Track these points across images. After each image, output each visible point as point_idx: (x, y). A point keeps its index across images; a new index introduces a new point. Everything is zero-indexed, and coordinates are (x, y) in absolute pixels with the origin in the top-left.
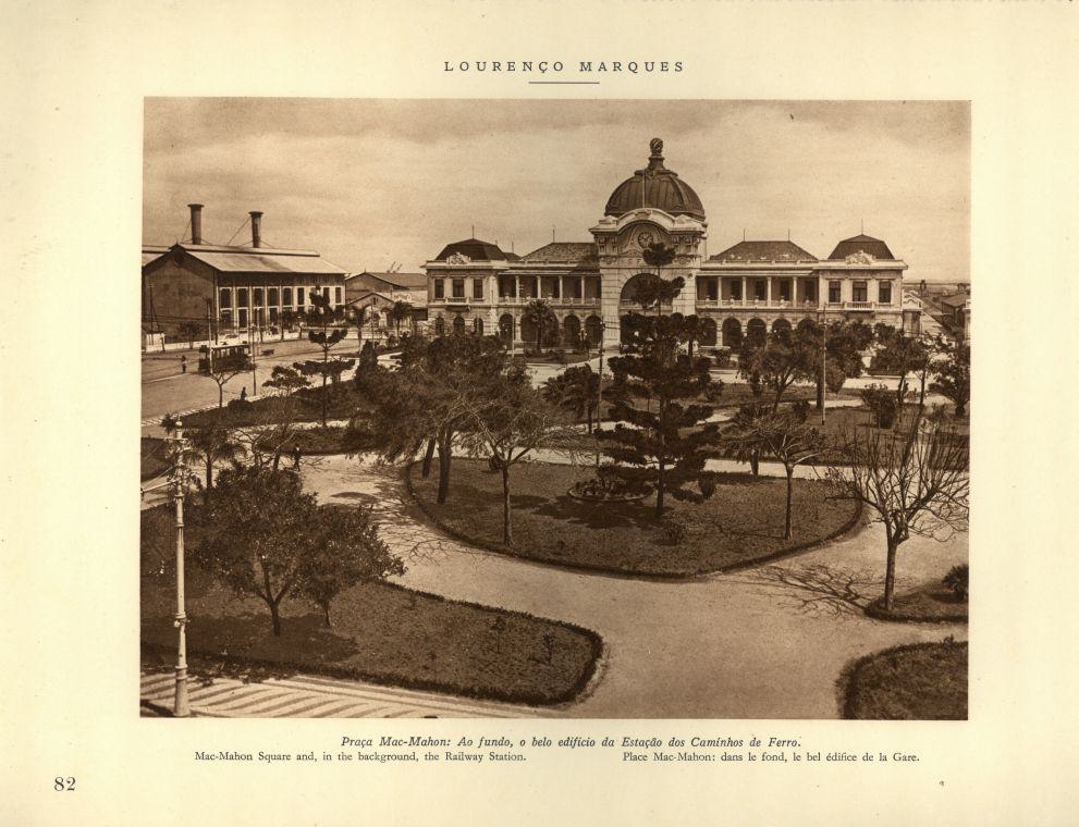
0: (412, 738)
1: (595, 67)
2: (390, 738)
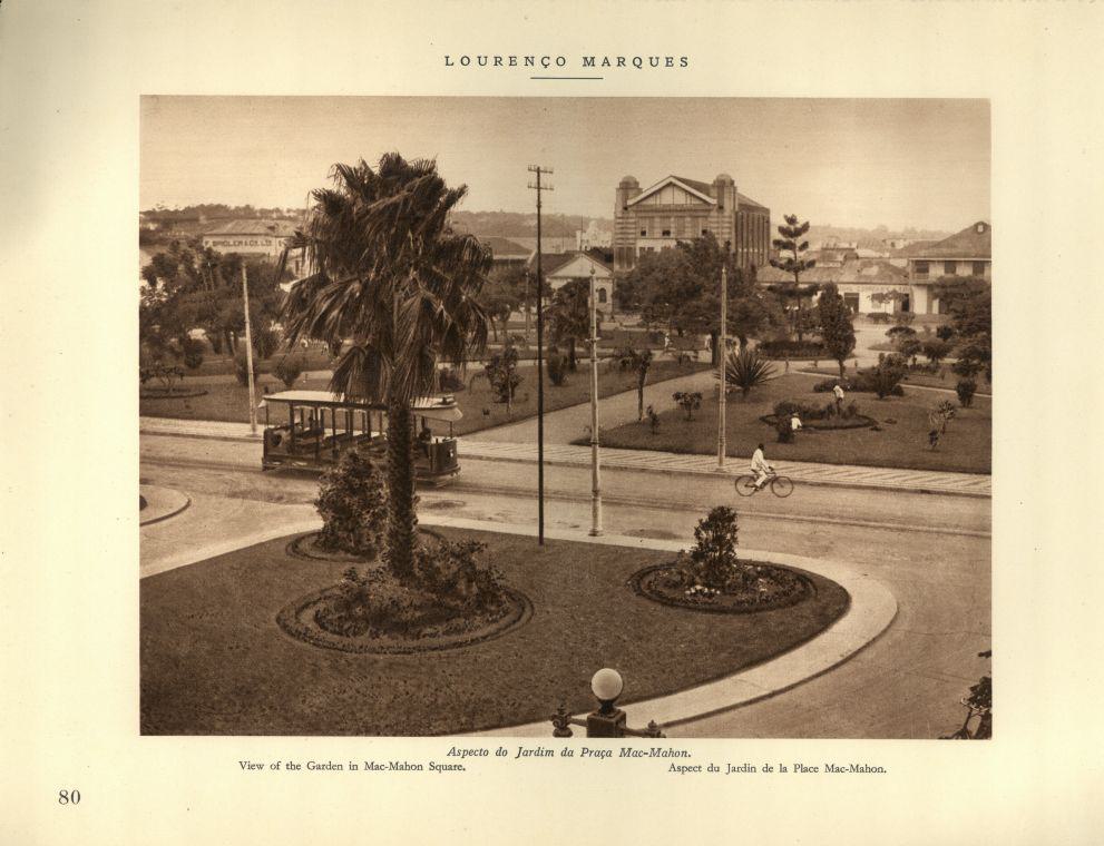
0: (653, 749)
1: (599, 62)
2: (660, 749)
